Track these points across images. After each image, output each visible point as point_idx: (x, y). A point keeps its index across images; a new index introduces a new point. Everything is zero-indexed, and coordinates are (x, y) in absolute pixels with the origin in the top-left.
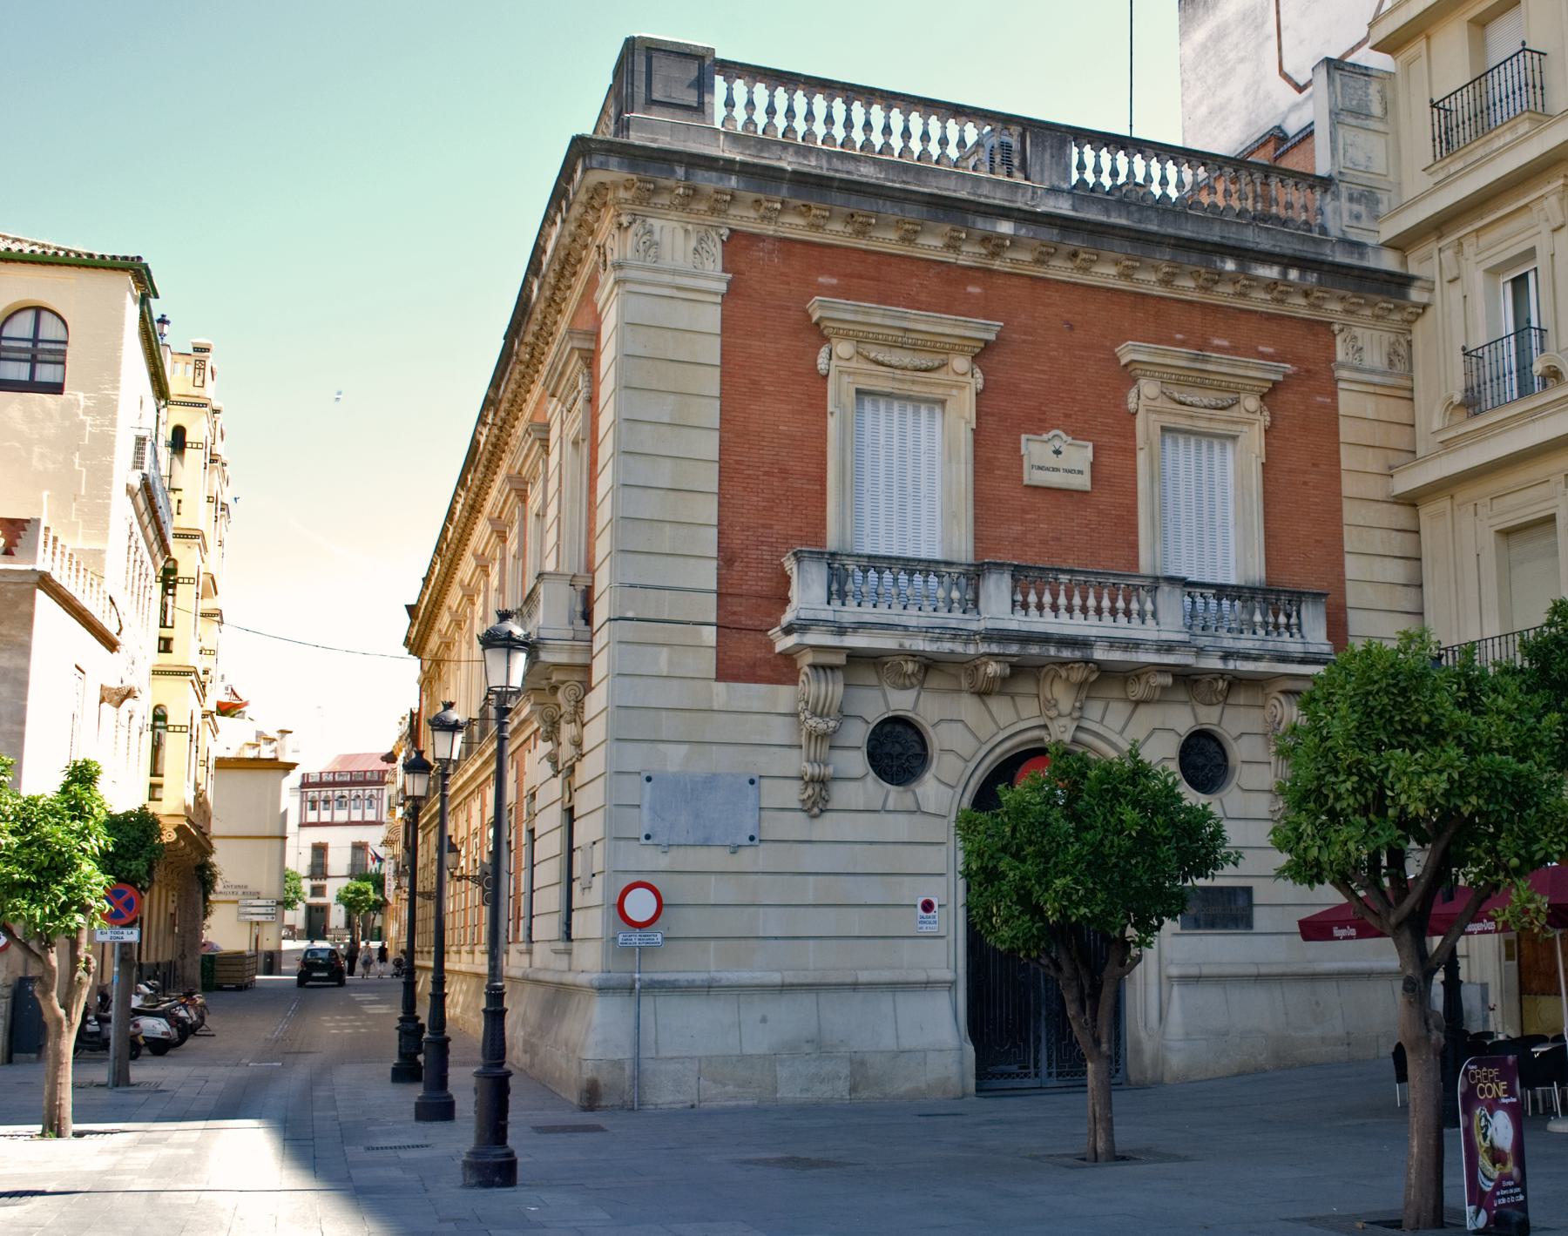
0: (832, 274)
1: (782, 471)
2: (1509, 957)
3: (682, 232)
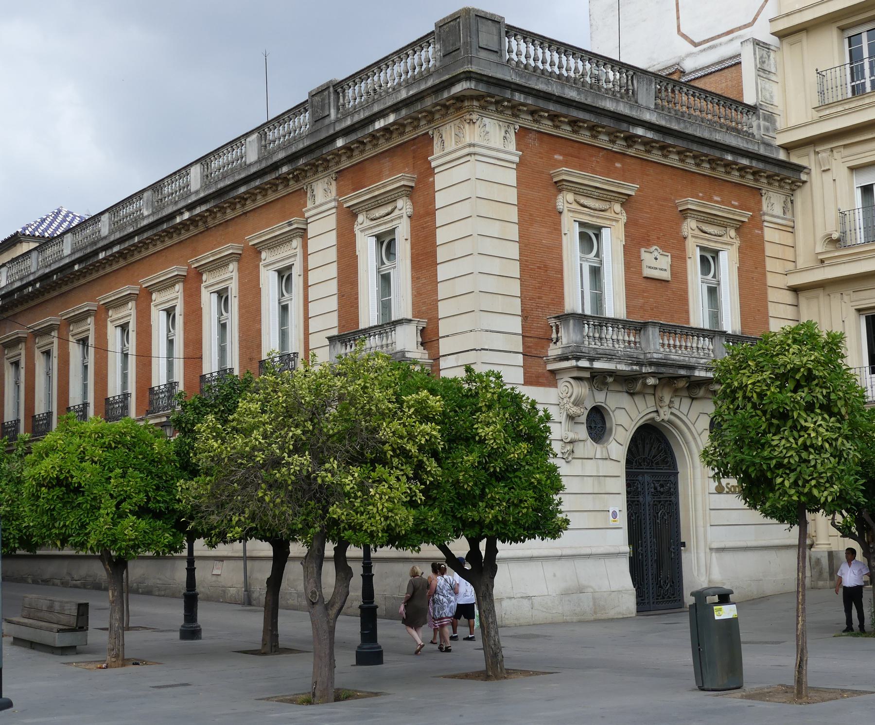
0: (560, 154)
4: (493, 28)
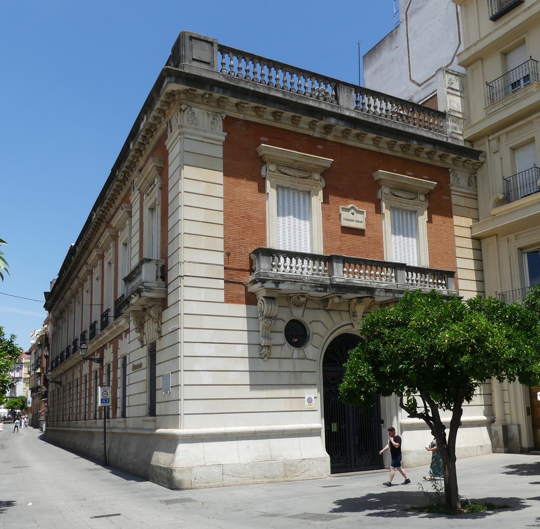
1: (248, 216)
2: (528, 414)
3: (206, 115)
4: (207, 46)
